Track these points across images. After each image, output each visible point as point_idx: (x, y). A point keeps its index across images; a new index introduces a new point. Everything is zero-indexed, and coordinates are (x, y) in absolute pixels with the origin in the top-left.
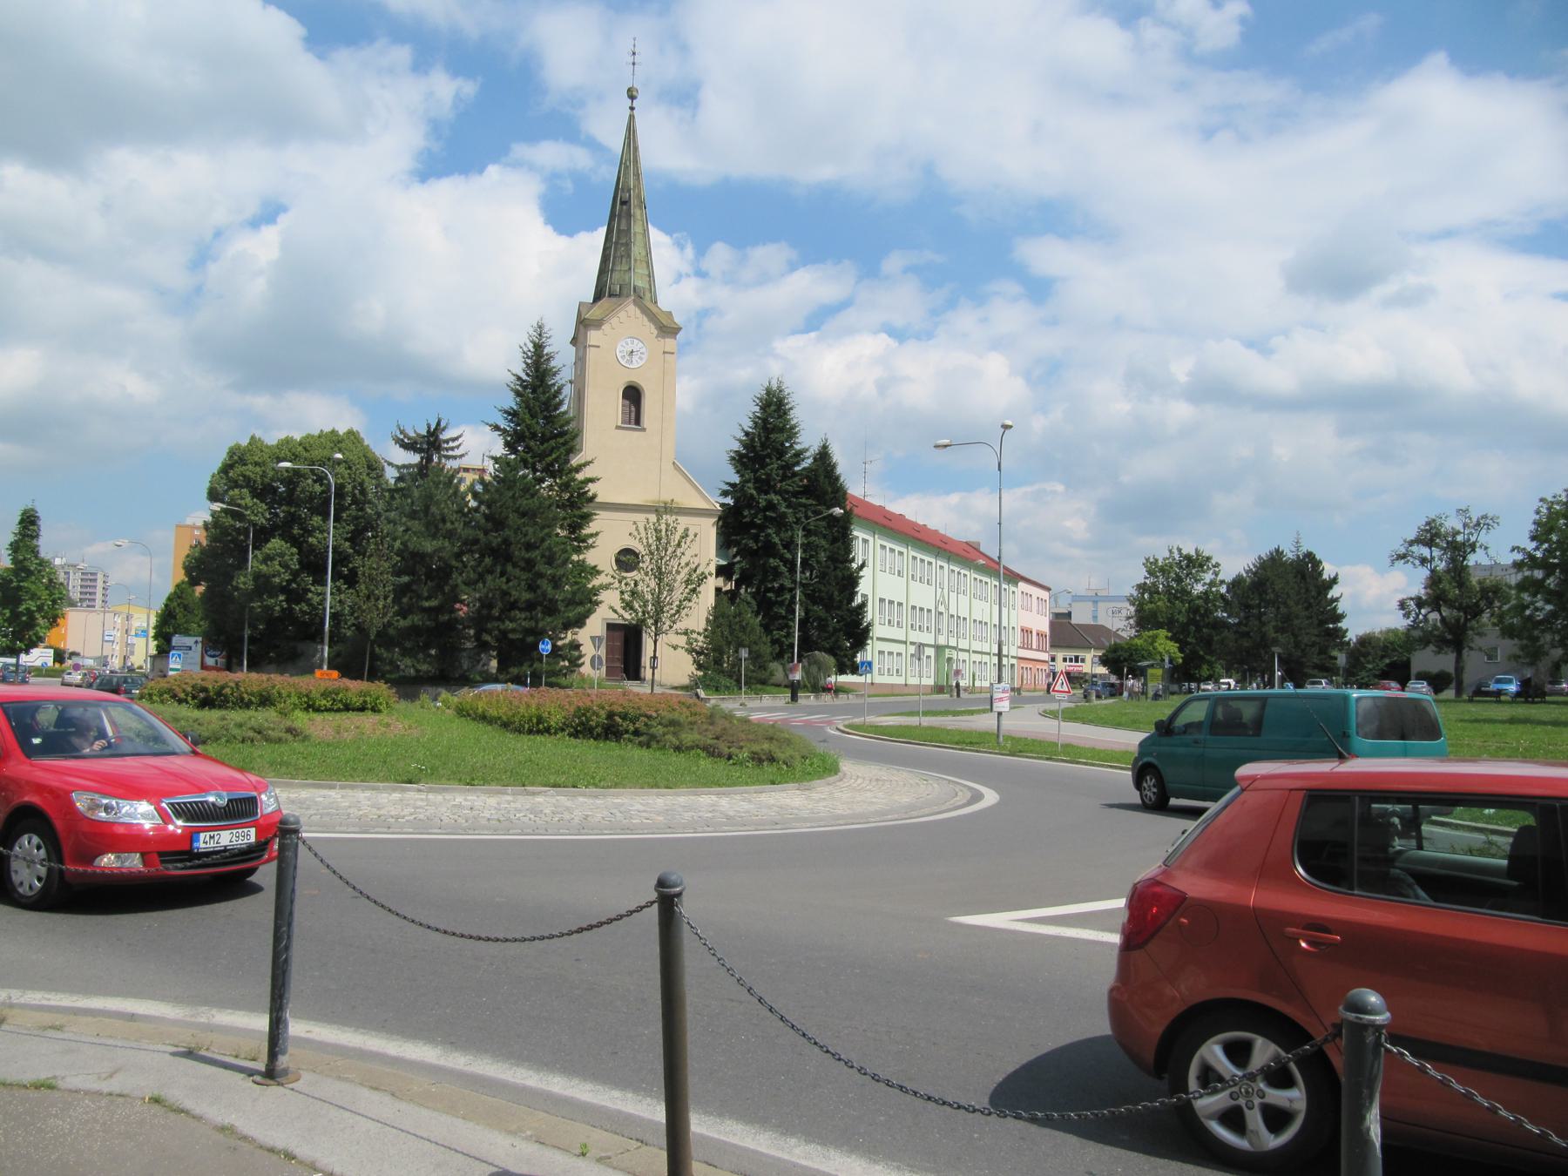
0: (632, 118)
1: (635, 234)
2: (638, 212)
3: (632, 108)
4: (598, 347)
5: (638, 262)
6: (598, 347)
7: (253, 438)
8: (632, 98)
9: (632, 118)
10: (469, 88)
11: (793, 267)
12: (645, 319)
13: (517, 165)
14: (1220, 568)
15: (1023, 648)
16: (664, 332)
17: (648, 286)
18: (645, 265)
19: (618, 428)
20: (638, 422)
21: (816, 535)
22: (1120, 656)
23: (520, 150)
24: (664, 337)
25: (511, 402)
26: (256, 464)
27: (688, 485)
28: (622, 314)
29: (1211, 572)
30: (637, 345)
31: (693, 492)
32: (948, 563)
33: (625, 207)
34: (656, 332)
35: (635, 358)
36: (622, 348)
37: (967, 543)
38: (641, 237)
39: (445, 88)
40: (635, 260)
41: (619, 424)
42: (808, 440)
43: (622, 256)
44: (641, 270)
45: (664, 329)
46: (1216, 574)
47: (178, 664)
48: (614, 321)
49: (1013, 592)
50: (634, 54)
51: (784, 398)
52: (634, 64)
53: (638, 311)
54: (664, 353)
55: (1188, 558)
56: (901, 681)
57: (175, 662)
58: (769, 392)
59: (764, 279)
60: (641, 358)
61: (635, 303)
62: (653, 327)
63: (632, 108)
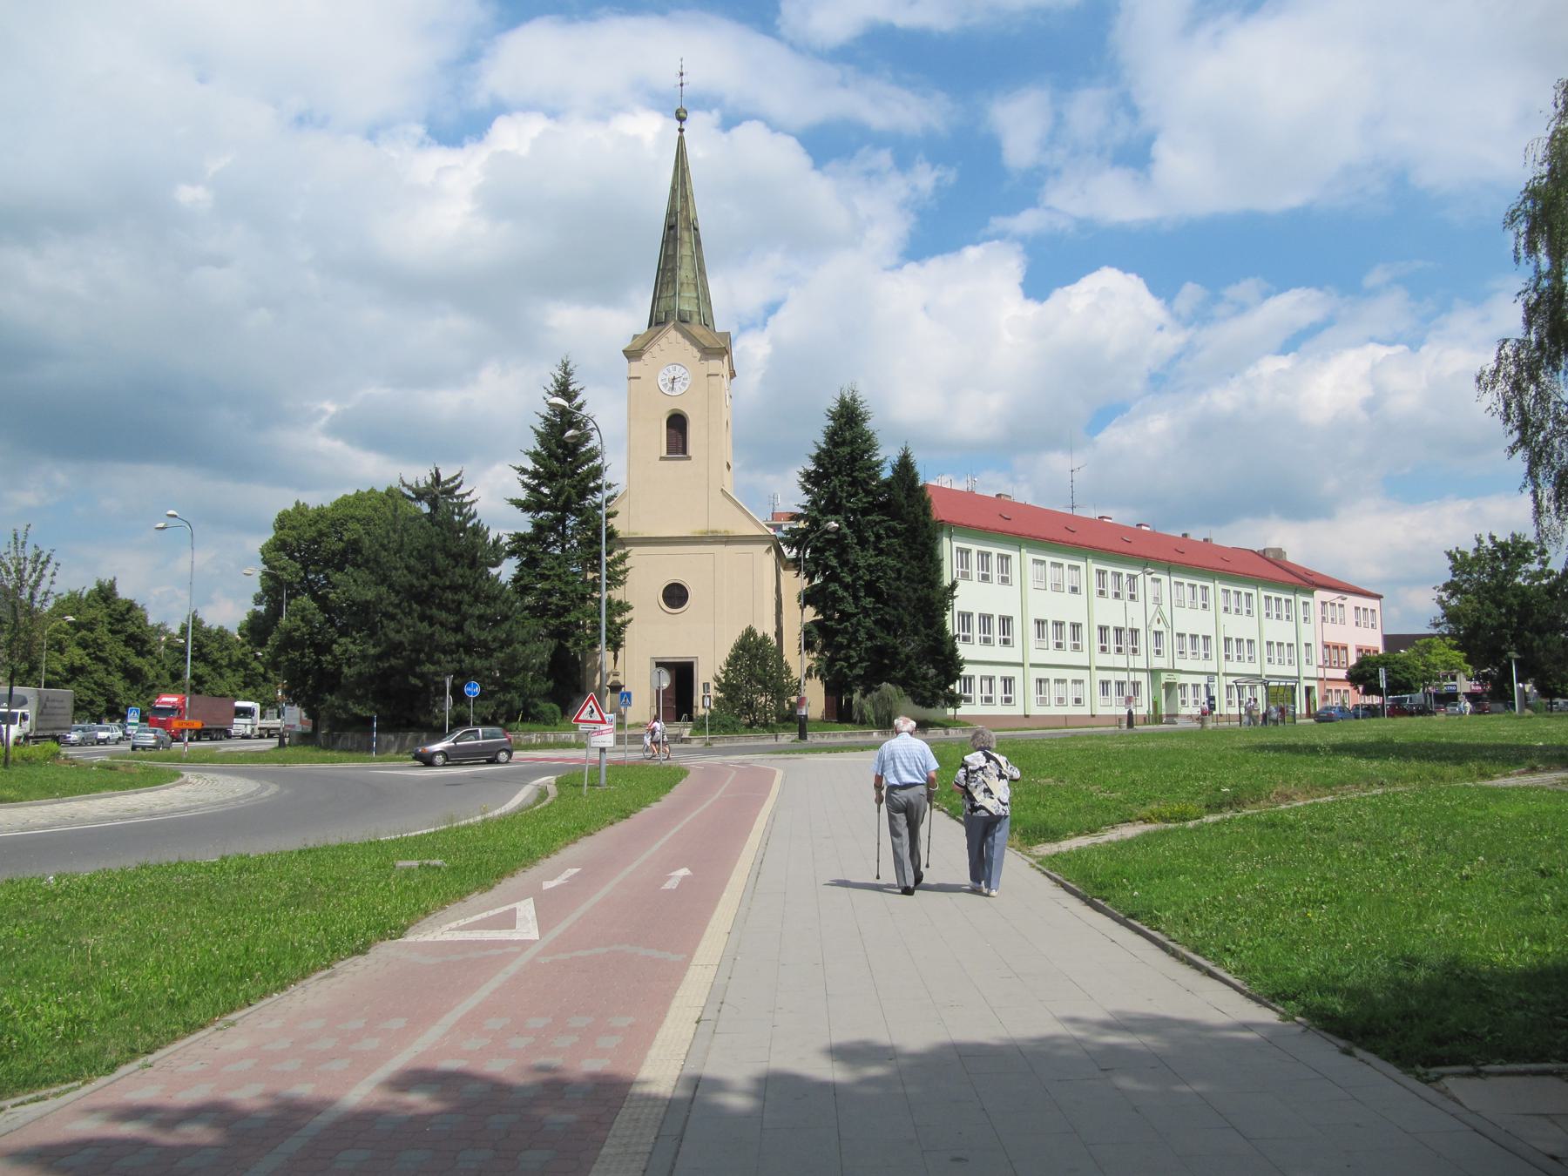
0: (681, 139)
1: (681, 258)
2: (686, 235)
3: (681, 130)
4: (639, 378)
5: (685, 285)
6: (639, 378)
7: (297, 503)
8: (681, 120)
9: (681, 139)
10: (952, 176)
11: (1266, 295)
12: (687, 343)
13: (1001, 236)
14: (478, 517)
15: (1330, 667)
16: (707, 354)
17: (696, 310)
18: (692, 287)
19: (662, 458)
20: (684, 451)
21: (888, 555)
22: (1365, 672)
23: (998, 223)
24: (707, 360)
25: (534, 444)
26: (294, 528)
27: (739, 513)
28: (663, 342)
29: (1537, 561)
30: (679, 372)
31: (746, 519)
32: (1169, 574)
33: (672, 232)
34: (698, 355)
35: (677, 385)
36: (663, 377)
37: (1262, 555)
38: (689, 258)
39: (925, 178)
40: (682, 284)
41: (664, 454)
42: (886, 455)
43: (668, 282)
44: (689, 293)
45: (707, 351)
46: (1545, 563)
47: (135, 718)
48: (655, 349)
49: (1305, 604)
50: (682, 74)
51: (857, 409)
52: (682, 85)
53: (679, 336)
54: (708, 375)
55: (1502, 547)
56: (1084, 711)
57: (134, 717)
58: (843, 404)
59: (1242, 309)
60: (684, 384)
61: (676, 328)
62: (695, 350)
63: (681, 130)
